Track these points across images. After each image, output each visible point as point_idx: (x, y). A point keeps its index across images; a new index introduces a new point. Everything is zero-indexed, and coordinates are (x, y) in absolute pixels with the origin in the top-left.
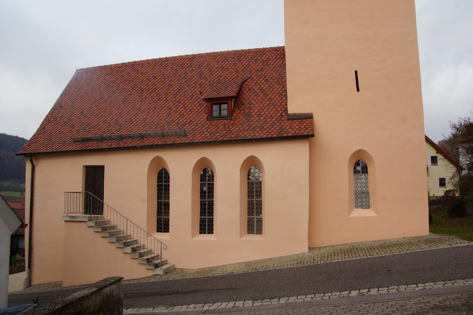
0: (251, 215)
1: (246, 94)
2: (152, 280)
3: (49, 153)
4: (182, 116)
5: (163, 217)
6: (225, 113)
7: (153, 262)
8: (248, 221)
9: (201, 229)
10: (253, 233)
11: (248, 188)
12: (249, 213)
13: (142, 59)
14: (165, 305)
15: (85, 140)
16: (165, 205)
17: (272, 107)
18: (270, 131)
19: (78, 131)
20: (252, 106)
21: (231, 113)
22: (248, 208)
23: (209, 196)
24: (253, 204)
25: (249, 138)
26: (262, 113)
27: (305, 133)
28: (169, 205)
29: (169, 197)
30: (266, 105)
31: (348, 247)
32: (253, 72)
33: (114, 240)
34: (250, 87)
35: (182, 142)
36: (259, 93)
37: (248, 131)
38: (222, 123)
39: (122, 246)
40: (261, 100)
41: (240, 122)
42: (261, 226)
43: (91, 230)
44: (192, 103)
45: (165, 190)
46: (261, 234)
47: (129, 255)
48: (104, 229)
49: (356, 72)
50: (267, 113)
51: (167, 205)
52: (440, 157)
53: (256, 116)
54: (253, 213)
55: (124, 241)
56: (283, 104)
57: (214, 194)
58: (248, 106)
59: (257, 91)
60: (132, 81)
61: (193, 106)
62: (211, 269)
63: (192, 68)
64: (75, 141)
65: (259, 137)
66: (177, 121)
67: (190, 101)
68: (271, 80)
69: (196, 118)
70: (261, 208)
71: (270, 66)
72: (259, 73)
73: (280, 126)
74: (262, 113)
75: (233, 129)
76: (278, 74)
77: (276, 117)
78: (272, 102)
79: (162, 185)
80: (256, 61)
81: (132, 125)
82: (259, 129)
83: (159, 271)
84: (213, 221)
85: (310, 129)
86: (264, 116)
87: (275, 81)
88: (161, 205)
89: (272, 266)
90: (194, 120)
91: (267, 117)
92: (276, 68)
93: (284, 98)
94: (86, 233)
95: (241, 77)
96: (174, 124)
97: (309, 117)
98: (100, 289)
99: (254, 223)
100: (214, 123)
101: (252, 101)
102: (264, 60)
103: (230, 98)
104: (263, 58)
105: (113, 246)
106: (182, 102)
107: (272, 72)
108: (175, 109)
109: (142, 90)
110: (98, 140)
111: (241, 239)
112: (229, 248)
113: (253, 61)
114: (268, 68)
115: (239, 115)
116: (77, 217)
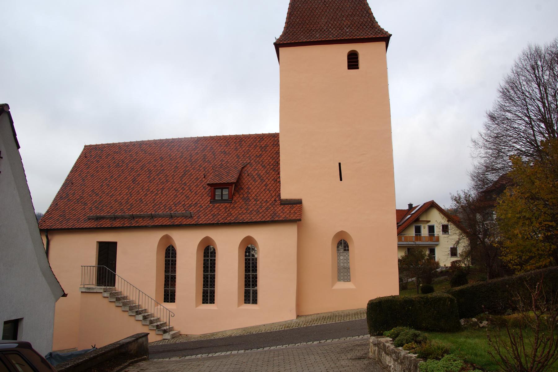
0: (248, 287)
1: (246, 179)
2: (161, 344)
3: (65, 229)
4: (188, 198)
5: (170, 288)
6: (226, 197)
7: (162, 328)
8: (245, 293)
9: (203, 300)
10: (249, 303)
11: (246, 263)
12: (246, 285)
13: (150, 139)
14: (178, 356)
15: (98, 218)
16: (172, 278)
17: (268, 192)
18: (265, 215)
19: (91, 209)
20: (250, 191)
21: (231, 196)
22: (245, 281)
23: (211, 271)
24: (249, 278)
25: (246, 221)
26: (259, 198)
27: (294, 218)
28: (175, 278)
29: (175, 271)
30: (262, 190)
31: (329, 314)
32: (253, 157)
33: (127, 309)
34: (249, 172)
35: (188, 223)
36: (257, 179)
37: (246, 214)
38: (224, 206)
39: (134, 314)
40: (258, 186)
41: (239, 206)
42: (256, 297)
43: (106, 300)
44: (197, 186)
45: (172, 264)
46: (256, 303)
47: (140, 323)
48: (118, 299)
49: (340, 164)
50: (263, 198)
51: (174, 278)
52: (451, 227)
53: (253, 200)
54: (249, 285)
55: (135, 310)
56: (277, 189)
57: (216, 269)
58: (247, 190)
59: (255, 177)
60: (140, 161)
61: (197, 189)
62: (213, 334)
63: (196, 151)
64: (89, 219)
65: (255, 220)
66: (183, 203)
67: (195, 184)
68: (268, 167)
69: (201, 200)
70: (256, 281)
71: (267, 152)
72: (258, 159)
73: (273, 211)
74: (259, 198)
75: (233, 212)
76: (274, 160)
77: (271, 202)
78: (268, 187)
79: (169, 260)
80: (256, 146)
81: (142, 205)
82: (255, 213)
83: (167, 336)
84: (214, 293)
85: (298, 213)
86: (260, 200)
87: (272, 167)
88: (168, 278)
89: (264, 330)
90: (199, 202)
91: (263, 202)
92: (273, 154)
93: (278, 184)
94: (100, 302)
95: (241, 162)
96: (181, 205)
97: (299, 202)
98: (137, 339)
99: (250, 295)
100: (217, 206)
101: (250, 186)
102: (263, 146)
103: (231, 184)
104: (261, 143)
105: (126, 314)
106: (188, 185)
107: (269, 158)
108: (181, 191)
109: (150, 171)
110: (111, 218)
111: (240, 308)
112: (229, 315)
113: (253, 146)
114: (265, 154)
115: (239, 199)
116: (93, 289)
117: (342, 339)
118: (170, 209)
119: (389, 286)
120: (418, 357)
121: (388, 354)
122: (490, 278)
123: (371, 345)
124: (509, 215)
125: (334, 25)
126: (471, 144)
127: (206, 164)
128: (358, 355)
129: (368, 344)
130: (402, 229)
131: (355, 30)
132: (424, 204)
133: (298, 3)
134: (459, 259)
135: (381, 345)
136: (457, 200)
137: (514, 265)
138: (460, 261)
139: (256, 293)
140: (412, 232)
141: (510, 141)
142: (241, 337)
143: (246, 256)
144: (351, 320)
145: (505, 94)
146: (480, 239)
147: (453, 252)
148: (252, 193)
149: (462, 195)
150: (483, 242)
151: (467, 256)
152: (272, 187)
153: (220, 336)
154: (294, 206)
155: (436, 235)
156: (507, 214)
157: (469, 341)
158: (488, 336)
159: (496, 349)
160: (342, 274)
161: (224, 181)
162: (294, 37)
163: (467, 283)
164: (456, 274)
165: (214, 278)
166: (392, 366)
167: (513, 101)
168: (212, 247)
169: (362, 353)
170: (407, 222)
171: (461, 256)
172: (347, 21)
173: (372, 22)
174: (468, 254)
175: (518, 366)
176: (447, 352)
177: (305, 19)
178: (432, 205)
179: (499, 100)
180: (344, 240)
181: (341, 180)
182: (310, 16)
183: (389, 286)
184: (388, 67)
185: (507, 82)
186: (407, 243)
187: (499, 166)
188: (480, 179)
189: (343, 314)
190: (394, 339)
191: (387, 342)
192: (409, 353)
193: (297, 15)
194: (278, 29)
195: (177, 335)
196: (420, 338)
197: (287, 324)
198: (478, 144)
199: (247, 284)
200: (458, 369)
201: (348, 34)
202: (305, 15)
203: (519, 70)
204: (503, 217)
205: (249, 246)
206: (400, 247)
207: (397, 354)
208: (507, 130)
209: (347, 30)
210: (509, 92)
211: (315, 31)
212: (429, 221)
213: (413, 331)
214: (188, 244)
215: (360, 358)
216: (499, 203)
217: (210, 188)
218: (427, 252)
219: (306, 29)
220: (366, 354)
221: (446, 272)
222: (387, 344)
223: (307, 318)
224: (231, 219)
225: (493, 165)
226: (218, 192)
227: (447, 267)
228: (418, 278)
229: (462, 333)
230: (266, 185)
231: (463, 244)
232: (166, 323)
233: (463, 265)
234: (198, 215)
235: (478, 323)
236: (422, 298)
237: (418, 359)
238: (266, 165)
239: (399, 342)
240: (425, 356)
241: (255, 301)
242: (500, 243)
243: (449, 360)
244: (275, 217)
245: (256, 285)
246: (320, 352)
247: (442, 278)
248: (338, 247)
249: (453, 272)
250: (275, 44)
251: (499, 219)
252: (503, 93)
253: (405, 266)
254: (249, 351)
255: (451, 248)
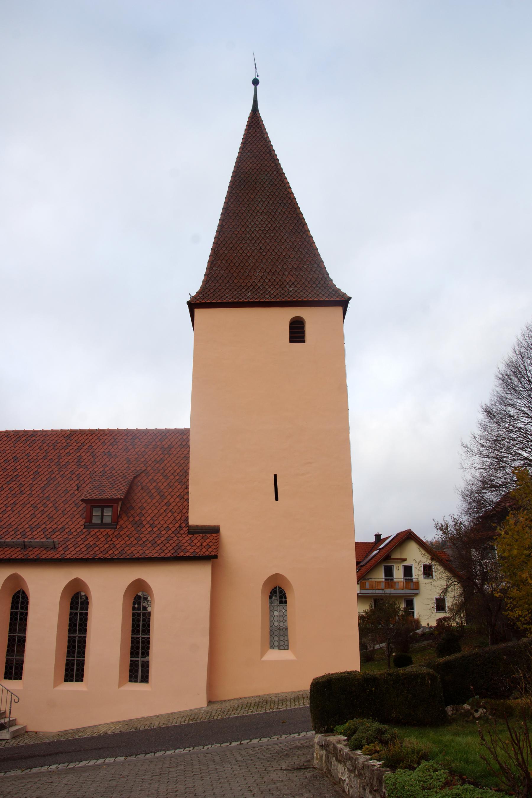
0: (135, 657)
6: (108, 520)
8: (131, 665)
9: (66, 675)
10: (136, 681)
11: (133, 620)
14: (19, 768)
16: (19, 641)
17: (170, 514)
18: (165, 548)
20: (143, 512)
21: (116, 519)
22: (132, 648)
23: (80, 630)
25: (137, 556)
26: (156, 523)
27: (207, 553)
28: (24, 641)
31: (257, 700)
34: (144, 484)
35: (50, 557)
36: (155, 494)
37: (137, 546)
38: (104, 534)
41: (127, 533)
45: (21, 619)
46: (147, 682)
49: (275, 476)
50: (162, 522)
51: (22, 641)
52: (437, 568)
56: (184, 511)
57: (88, 628)
59: (153, 491)
61: (66, 506)
62: (78, 731)
63: (68, 450)
65: (149, 555)
66: (44, 526)
67: (64, 499)
68: (172, 477)
69: (70, 523)
70: (148, 648)
71: (171, 456)
72: (157, 465)
73: (177, 542)
75: (117, 542)
76: (181, 468)
78: (171, 507)
82: (150, 545)
85: (213, 547)
86: (159, 526)
87: (177, 478)
88: (14, 640)
90: (67, 526)
91: (162, 529)
92: (179, 459)
93: (185, 503)
95: (132, 469)
96: (40, 529)
97: (215, 530)
100: (93, 533)
101: (145, 505)
102: (166, 446)
103: (116, 501)
106: (52, 499)
108: (42, 508)
112: (105, 700)
113: (150, 447)
114: (169, 459)
115: (127, 523)
117: (274, 739)
118: (24, 535)
119: (345, 657)
120: (384, 766)
121: (340, 762)
122: (492, 644)
123: (317, 747)
124: (515, 552)
125: (272, 281)
126: (462, 450)
127: (82, 469)
128: (297, 763)
129: (313, 746)
130: (364, 570)
131: (301, 289)
132: (398, 535)
133: (224, 249)
134: (448, 615)
135: (331, 747)
136: (443, 528)
137: (524, 624)
138: (449, 618)
139: (148, 666)
140: (380, 576)
141: (515, 446)
142: (121, 734)
143: (134, 608)
144: (288, 708)
145: (505, 381)
146: (477, 586)
147: (440, 605)
148: (146, 515)
149: (451, 523)
150: (481, 590)
151: (459, 611)
152: (176, 508)
153: (89, 734)
154: (208, 535)
155: (414, 580)
156: (512, 550)
157: (459, 739)
158: (480, 732)
159: (491, 751)
160: (276, 638)
161: (107, 496)
162: (216, 295)
163: (459, 650)
164: (444, 637)
165: (85, 642)
166: (347, 780)
167: (516, 391)
168: (83, 594)
169: (303, 760)
170: (373, 561)
171: (451, 610)
172: (290, 277)
173: (324, 280)
174: (459, 608)
175: (524, 778)
176: (425, 757)
177: (232, 271)
178: (407, 537)
179: (498, 389)
180: (280, 588)
181: (277, 499)
182: (240, 268)
183: (345, 657)
184: (346, 341)
185: (508, 366)
186: (374, 591)
187: (500, 481)
188: (475, 500)
189: (276, 699)
190: (349, 737)
191: (339, 742)
192: (371, 759)
193: (222, 265)
194: (194, 282)
195: (24, 732)
196: (387, 736)
197: (193, 715)
198: (471, 450)
199: (134, 652)
200: (440, 783)
201: (291, 294)
202: (232, 265)
203: (523, 350)
204: (505, 554)
205: (140, 594)
206: (361, 597)
207: (354, 761)
208: (510, 431)
209: (291, 289)
210: (511, 379)
211: (246, 288)
212: (405, 560)
213: (376, 725)
214: (45, 589)
215: (299, 769)
216: (500, 535)
217: (84, 505)
218: (403, 606)
219: (233, 285)
220: (309, 761)
221: (431, 634)
222: (339, 746)
223: (224, 705)
224: (116, 553)
225: (492, 481)
226: (97, 513)
227: (431, 627)
228: (388, 645)
229: (449, 728)
230: (168, 504)
231: (453, 593)
232: (4, 713)
233: (454, 624)
234: (65, 546)
235: (472, 711)
236: (390, 674)
237: (384, 769)
238: (169, 475)
239: (357, 743)
240: (393, 763)
241: (145, 679)
242: (504, 591)
243: (428, 770)
244: (179, 551)
245: (148, 654)
246: (241, 758)
247: (425, 643)
248: (271, 598)
249: (439, 634)
250: (188, 303)
251: (502, 558)
252: (503, 380)
253: (367, 627)
254: (132, 758)
255: (436, 599)
